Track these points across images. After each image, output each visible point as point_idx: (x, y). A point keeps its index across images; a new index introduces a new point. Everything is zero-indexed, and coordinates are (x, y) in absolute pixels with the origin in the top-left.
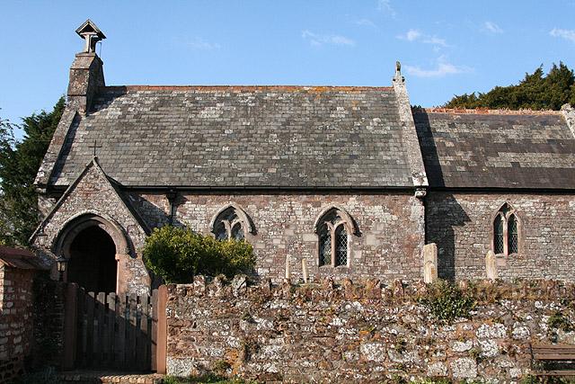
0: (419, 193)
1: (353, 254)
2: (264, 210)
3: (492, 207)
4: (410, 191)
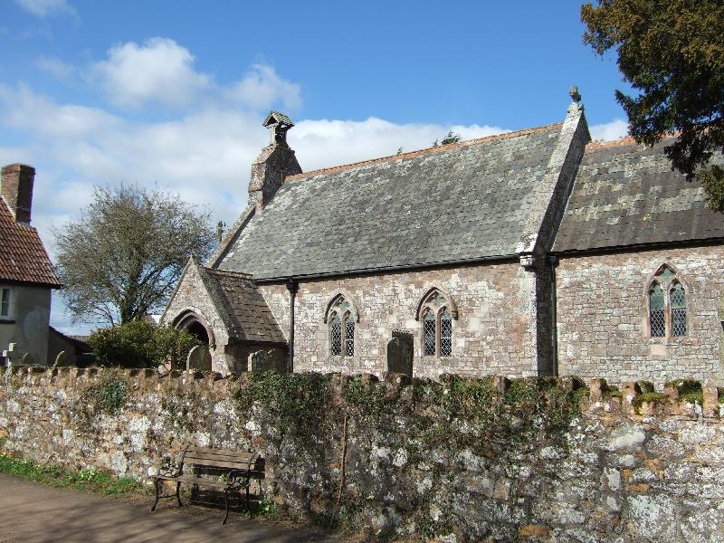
0: (524, 262)
1: (459, 343)
2: (370, 295)
3: (644, 272)
4: (514, 259)
